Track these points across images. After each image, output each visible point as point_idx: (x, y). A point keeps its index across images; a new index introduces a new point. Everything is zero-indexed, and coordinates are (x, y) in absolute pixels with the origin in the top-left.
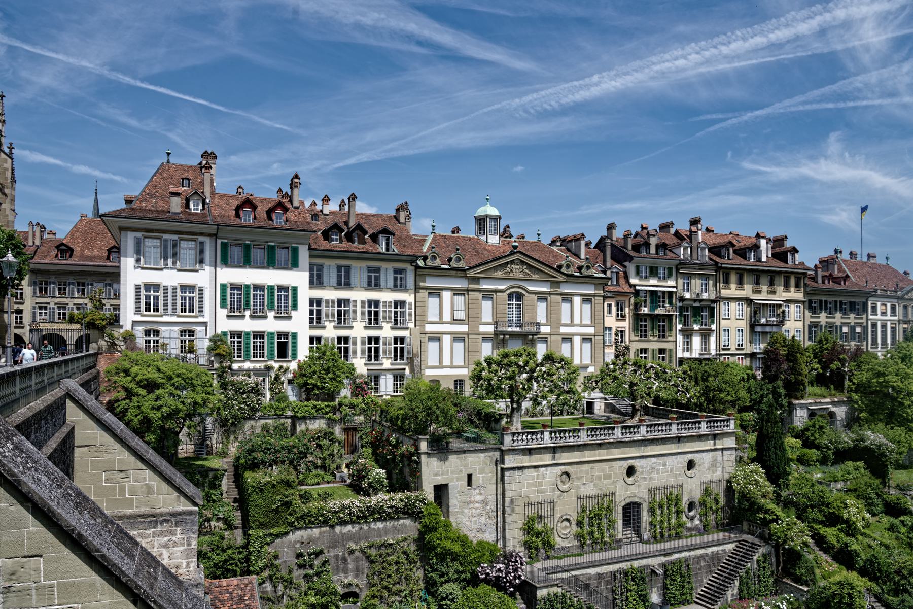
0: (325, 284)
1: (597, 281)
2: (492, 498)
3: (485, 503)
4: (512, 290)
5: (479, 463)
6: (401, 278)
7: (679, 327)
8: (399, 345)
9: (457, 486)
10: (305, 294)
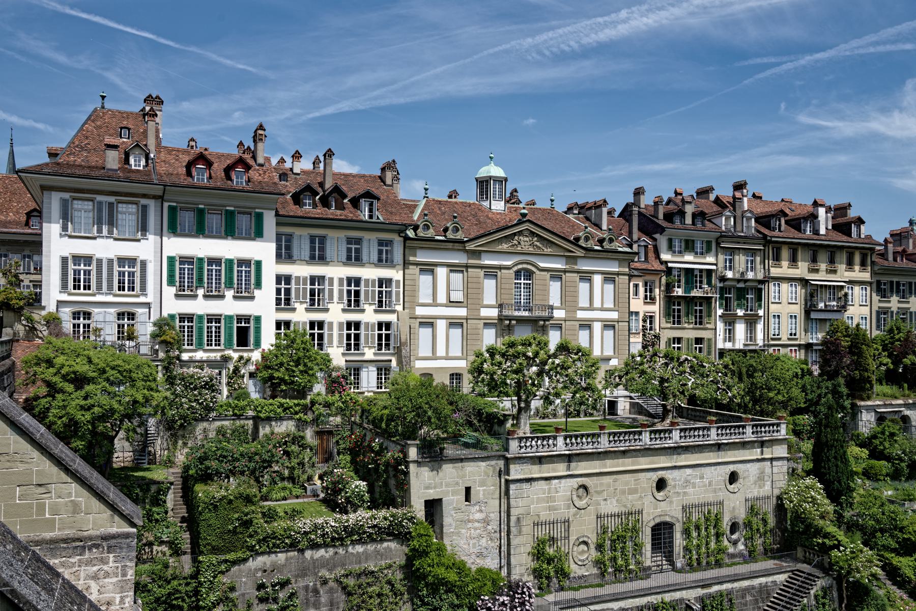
0: (295, 258)
1: (621, 256)
2: (494, 516)
3: (486, 521)
4: (520, 266)
5: (480, 474)
6: (387, 251)
7: (720, 312)
8: (384, 332)
9: (452, 501)
10: (271, 269)
